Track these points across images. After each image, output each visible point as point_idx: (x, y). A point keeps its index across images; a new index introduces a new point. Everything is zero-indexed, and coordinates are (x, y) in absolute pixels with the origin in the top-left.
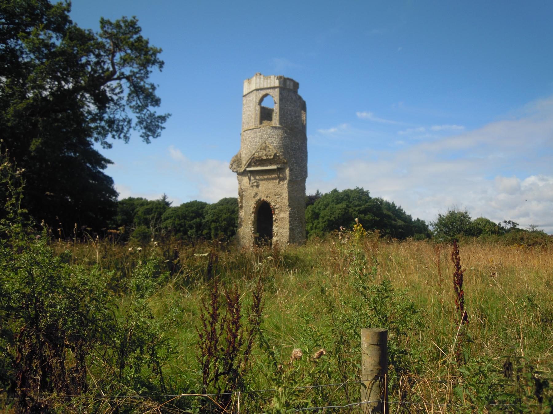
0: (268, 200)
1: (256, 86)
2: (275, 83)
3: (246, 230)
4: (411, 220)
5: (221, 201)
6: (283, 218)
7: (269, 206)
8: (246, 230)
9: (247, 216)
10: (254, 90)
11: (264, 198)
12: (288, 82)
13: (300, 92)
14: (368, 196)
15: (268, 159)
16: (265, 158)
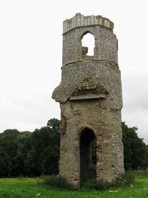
0: (90, 127)
1: (76, 24)
2: (94, 22)
3: (69, 165)
4: (58, 120)
5: (5, 131)
6: (106, 144)
7: (93, 133)
8: (69, 165)
9: (70, 145)
10: (75, 28)
11: (86, 125)
12: (106, 22)
13: (115, 31)
14: (124, 124)
15: (91, 89)
16: (88, 88)
